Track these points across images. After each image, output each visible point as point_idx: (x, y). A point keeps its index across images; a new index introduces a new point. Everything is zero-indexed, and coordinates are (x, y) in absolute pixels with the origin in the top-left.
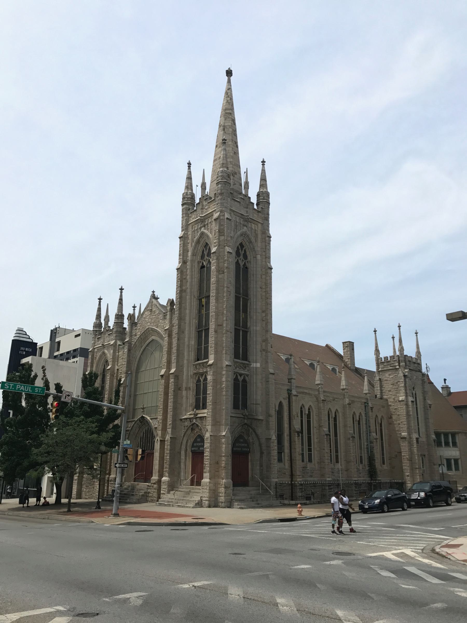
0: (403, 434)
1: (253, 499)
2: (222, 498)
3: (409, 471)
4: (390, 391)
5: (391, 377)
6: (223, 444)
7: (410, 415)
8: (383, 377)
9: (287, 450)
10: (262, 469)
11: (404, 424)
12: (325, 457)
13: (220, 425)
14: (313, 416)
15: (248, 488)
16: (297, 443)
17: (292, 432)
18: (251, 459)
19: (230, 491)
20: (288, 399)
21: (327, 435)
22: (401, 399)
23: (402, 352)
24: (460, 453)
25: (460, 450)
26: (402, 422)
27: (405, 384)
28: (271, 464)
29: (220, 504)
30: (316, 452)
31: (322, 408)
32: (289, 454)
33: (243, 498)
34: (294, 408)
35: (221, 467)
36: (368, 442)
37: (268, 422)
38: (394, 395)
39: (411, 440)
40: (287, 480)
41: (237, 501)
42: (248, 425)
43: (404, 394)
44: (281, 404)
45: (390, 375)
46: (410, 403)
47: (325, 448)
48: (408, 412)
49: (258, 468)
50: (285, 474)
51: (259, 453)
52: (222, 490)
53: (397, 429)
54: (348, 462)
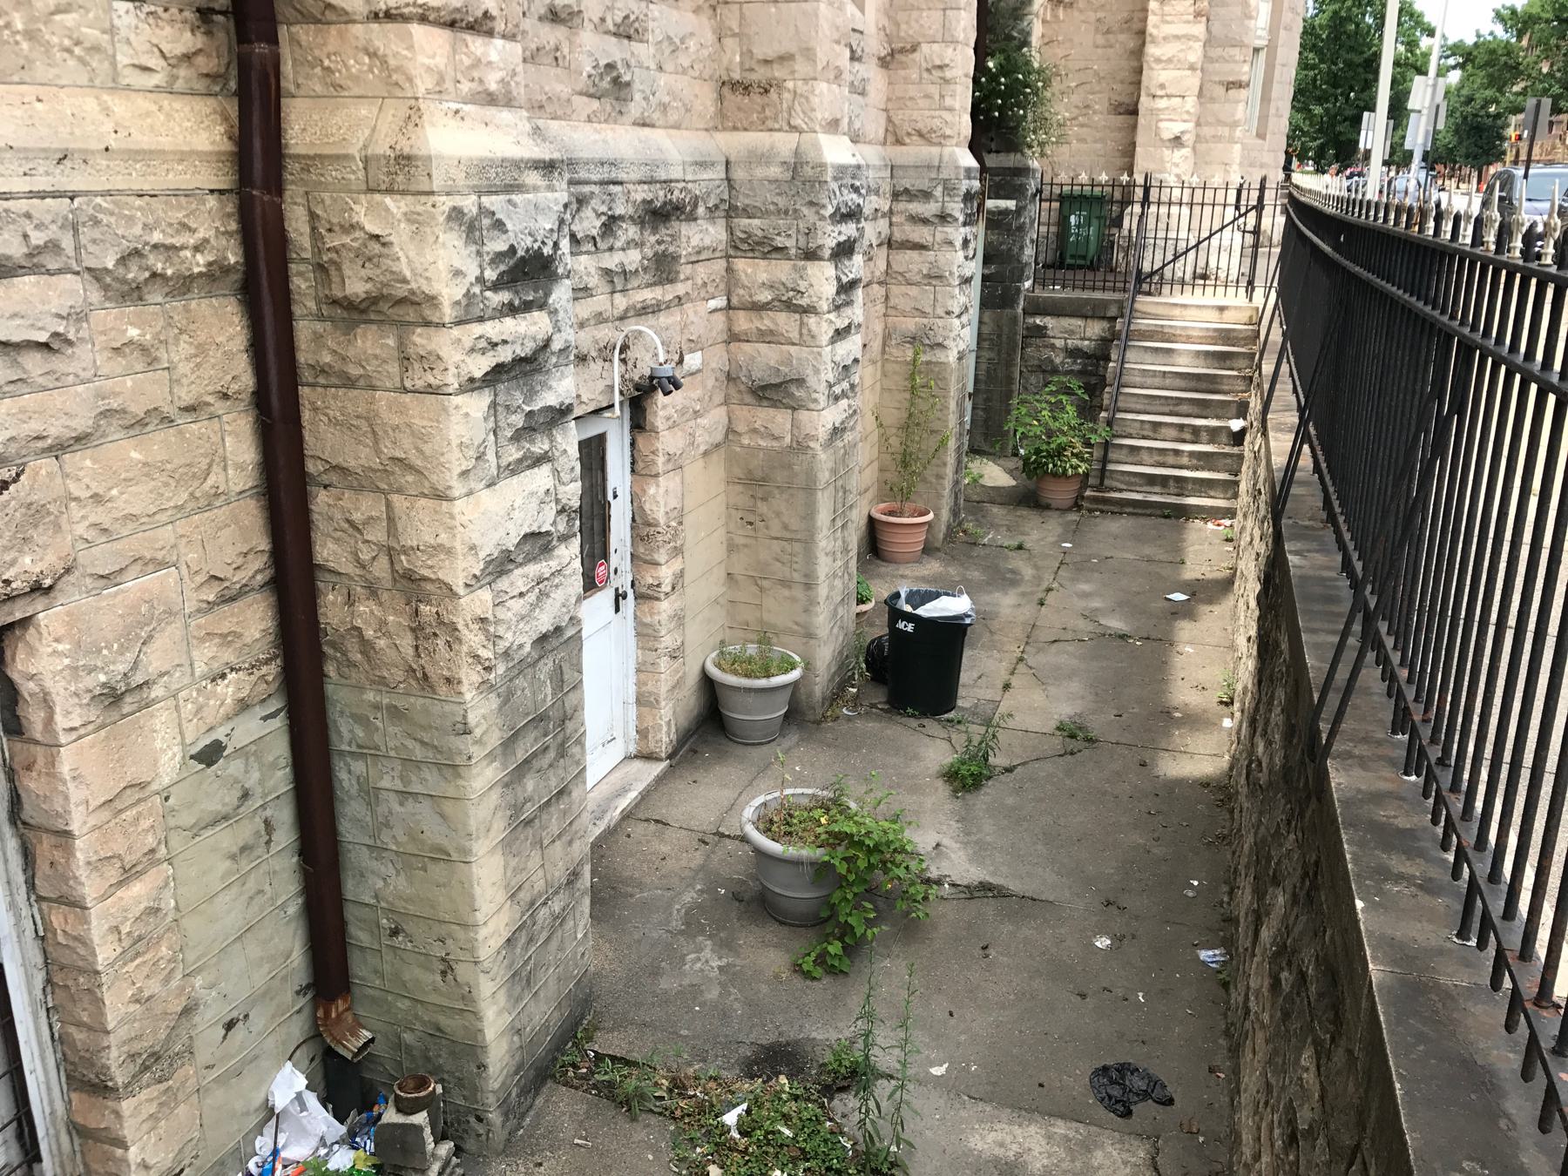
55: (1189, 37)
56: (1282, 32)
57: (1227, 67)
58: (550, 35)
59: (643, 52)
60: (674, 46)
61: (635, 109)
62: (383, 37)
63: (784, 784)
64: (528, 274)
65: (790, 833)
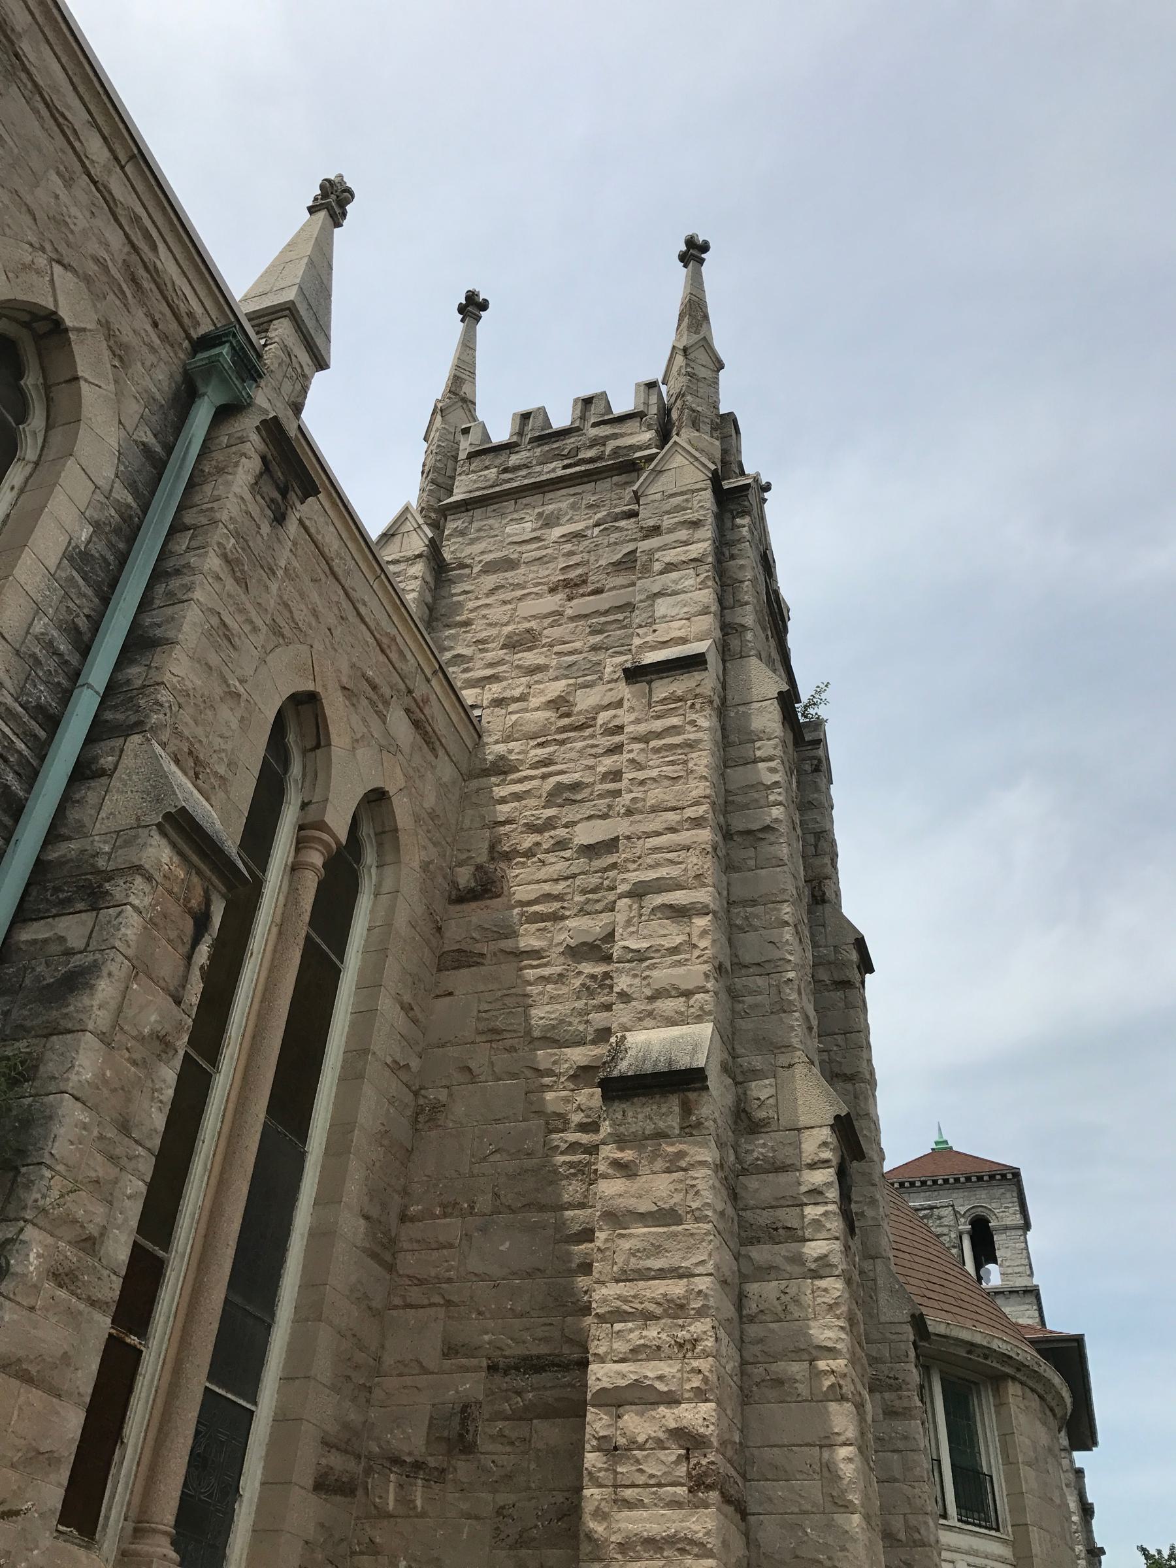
0: (637, 1039)
11: (680, 913)
22: (650, 1043)
26: (638, 892)
39: (760, 1148)
45: (549, 522)
53: (541, 1015)
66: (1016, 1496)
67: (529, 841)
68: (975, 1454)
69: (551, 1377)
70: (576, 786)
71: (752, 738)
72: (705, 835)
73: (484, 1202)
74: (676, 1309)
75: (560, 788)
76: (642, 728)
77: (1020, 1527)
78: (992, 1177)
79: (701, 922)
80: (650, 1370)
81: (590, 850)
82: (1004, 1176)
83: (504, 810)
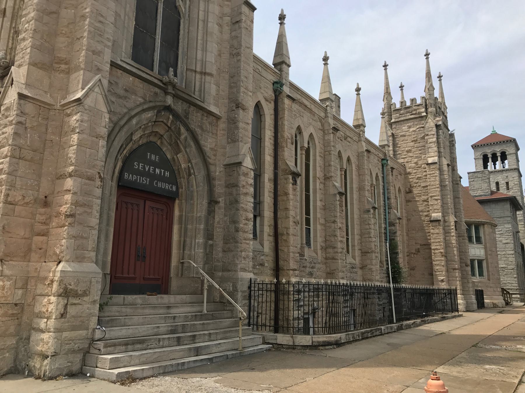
0: (433, 215)
1: (178, 334)
2: (45, 336)
3: (444, 273)
4: (408, 151)
5: (411, 130)
6: (73, 131)
7: (445, 186)
8: (399, 131)
9: (268, 213)
10: (212, 246)
11: (437, 200)
12: (335, 236)
13: (68, 72)
14: (315, 155)
15: (166, 299)
16: (291, 197)
17: (280, 173)
18: (180, 217)
19: (88, 307)
20: (273, 103)
21: (341, 194)
22: (430, 161)
23: (431, 92)
24: (486, 252)
25: (485, 248)
26: (431, 197)
27: (437, 139)
28: (237, 230)
29: (36, 363)
30: (319, 227)
31: (332, 144)
32: (272, 222)
33: (143, 330)
34: (286, 123)
35: (59, 214)
36: (386, 224)
37: (233, 122)
38: (417, 157)
39: (447, 224)
40: (267, 278)
41: (112, 345)
42: (176, 116)
43: (436, 154)
44: (258, 106)
45: (410, 127)
46: (445, 168)
47: (338, 220)
48: (442, 181)
49: (200, 240)
50: (262, 265)
51: (205, 202)
52: (51, 304)
53: (420, 209)
54: (364, 253)
55: (441, 260)
56: (489, 256)
57: (452, 266)
58: (303, 269)
59: (315, 270)
60: (319, 269)
61: (314, 277)
62: (288, 271)
63: (302, 277)
64: (299, 292)
65: (238, 73)
66: (485, 239)
67: (415, 185)
68: (479, 234)
69: (427, 246)
70: (420, 177)
71: (444, 171)
72: (439, 189)
73: (417, 229)
74: (439, 242)
75: (418, 177)
76: (429, 173)
77: (485, 243)
78: (507, 141)
79: (439, 201)
80: (437, 247)
81: (424, 187)
82: (511, 141)
83: (411, 180)
